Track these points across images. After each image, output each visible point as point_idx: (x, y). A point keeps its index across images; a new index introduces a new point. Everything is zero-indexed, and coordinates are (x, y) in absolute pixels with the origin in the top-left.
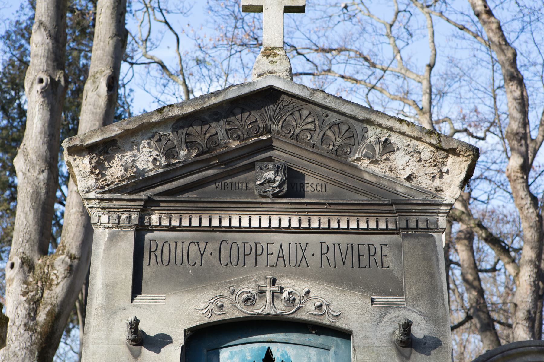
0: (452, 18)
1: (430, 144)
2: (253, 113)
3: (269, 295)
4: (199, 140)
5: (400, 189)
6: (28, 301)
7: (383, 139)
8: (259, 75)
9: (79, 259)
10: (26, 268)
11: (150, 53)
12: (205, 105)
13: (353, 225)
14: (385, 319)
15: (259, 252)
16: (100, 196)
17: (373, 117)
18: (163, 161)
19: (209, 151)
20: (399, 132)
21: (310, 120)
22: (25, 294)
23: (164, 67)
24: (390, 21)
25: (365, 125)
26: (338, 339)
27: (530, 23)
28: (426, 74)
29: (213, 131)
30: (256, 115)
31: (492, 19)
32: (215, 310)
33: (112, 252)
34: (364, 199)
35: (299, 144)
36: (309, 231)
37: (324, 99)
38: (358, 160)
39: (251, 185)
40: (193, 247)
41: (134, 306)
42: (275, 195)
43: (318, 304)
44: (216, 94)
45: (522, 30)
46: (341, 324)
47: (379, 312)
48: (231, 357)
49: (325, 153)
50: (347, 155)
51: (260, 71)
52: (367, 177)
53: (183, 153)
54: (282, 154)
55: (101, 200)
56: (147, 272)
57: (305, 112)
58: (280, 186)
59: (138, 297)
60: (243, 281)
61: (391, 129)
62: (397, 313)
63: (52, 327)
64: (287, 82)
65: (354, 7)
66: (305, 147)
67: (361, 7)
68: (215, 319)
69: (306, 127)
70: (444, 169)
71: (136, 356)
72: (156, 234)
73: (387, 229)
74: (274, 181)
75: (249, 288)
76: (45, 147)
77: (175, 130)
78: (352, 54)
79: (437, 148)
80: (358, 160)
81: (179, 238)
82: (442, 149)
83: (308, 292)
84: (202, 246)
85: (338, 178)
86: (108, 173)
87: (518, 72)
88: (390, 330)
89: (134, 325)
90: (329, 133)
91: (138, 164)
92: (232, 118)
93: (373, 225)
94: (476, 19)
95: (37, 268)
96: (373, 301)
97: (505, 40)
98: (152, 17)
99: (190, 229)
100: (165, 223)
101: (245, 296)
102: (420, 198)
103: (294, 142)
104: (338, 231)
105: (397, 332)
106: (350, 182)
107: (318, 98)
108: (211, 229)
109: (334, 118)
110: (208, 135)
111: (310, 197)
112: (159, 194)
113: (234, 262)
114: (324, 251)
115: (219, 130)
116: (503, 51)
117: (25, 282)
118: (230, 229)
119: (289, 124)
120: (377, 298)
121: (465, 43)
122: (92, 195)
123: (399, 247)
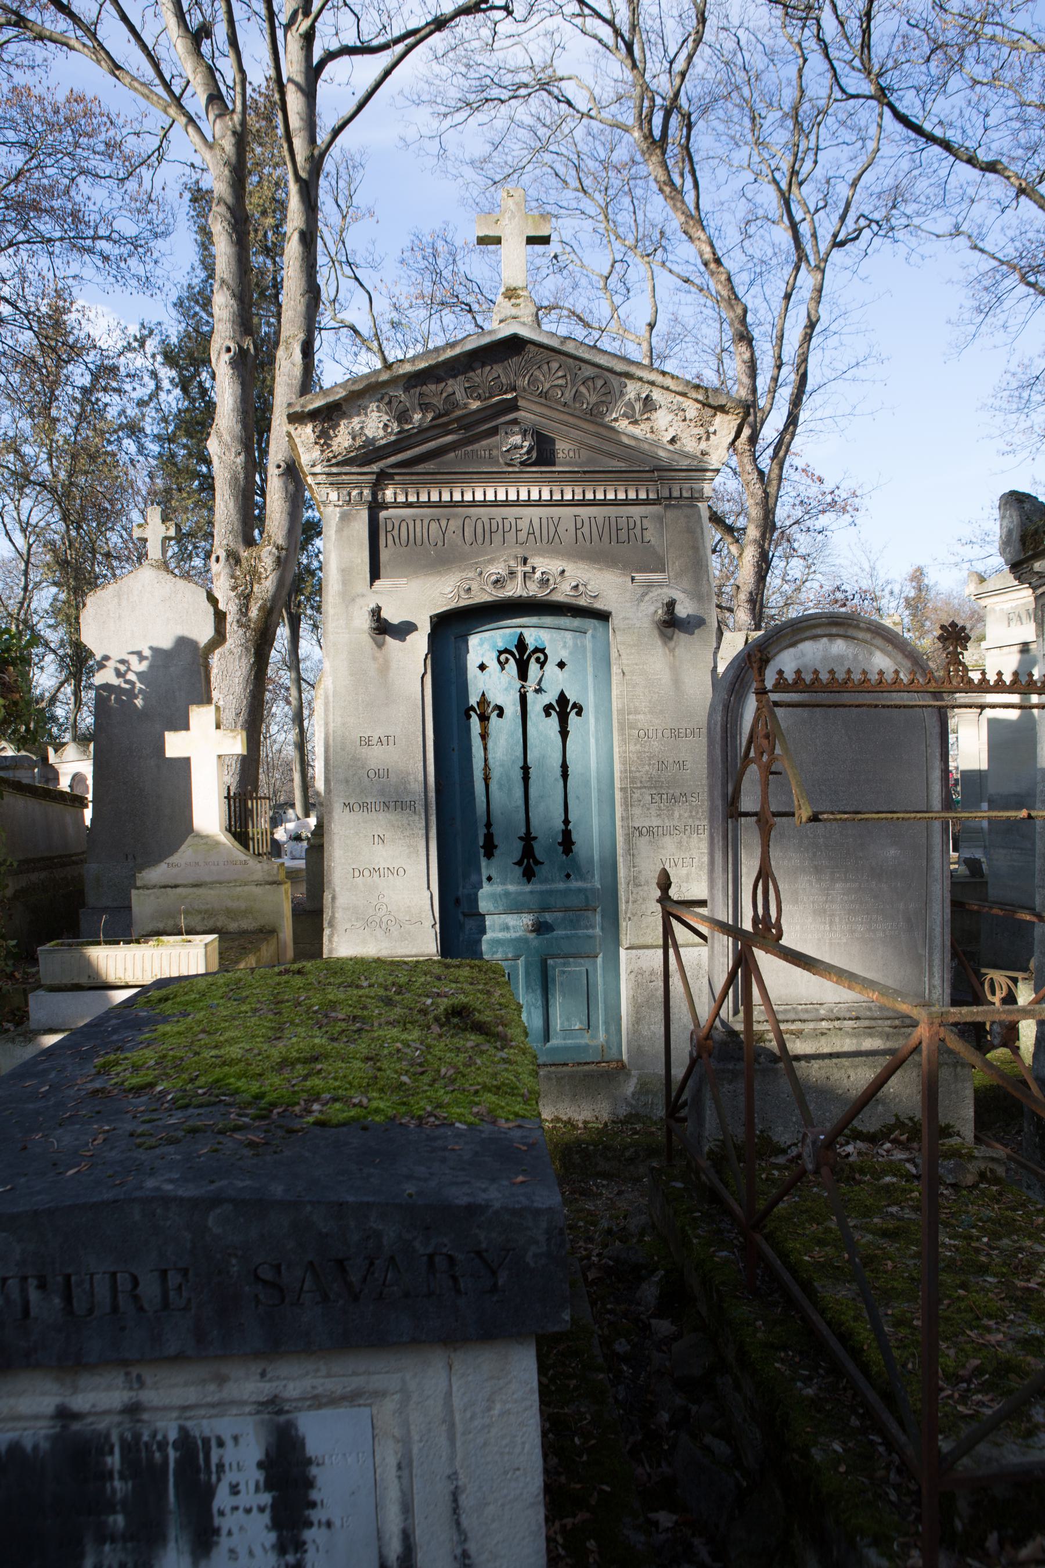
0: (676, 268)
1: (697, 400)
2: (495, 367)
3: (520, 575)
4: (434, 401)
5: (662, 453)
6: (238, 596)
7: (644, 396)
8: (501, 321)
9: (287, 550)
10: (232, 562)
11: (340, 316)
12: (440, 359)
13: (611, 496)
14: (647, 598)
15: (507, 529)
16: (327, 470)
17: (633, 370)
18: (395, 427)
19: (446, 414)
20: (662, 387)
21: (560, 374)
22: (234, 588)
23: (356, 331)
24: (606, 274)
25: (623, 379)
26: (595, 622)
27: (761, 273)
28: (647, 335)
29: (450, 390)
30: (498, 369)
31: (721, 269)
32: (462, 593)
33: (345, 533)
34: (622, 465)
35: (549, 403)
36: (562, 503)
37: (577, 349)
38: (616, 420)
39: (494, 452)
40: (434, 526)
41: (376, 592)
42: (523, 463)
43: (574, 584)
44: (452, 345)
45: (751, 284)
46: (599, 605)
47: (640, 591)
48: (481, 644)
49: (577, 413)
50: (603, 415)
51: (502, 316)
52: (625, 440)
53: (417, 417)
54: (529, 415)
55: (328, 474)
56: (384, 555)
57: (555, 365)
58: (528, 452)
59: (377, 583)
60: (491, 561)
61: (652, 383)
62: (660, 591)
63: (266, 622)
64: (534, 329)
65: (565, 257)
66: (555, 406)
67: (572, 256)
68: (463, 603)
69: (556, 383)
70: (711, 429)
71: (380, 645)
72: (391, 512)
73: (647, 499)
74: (522, 447)
75: (498, 569)
76: (240, 426)
77: (406, 390)
78: (565, 313)
79: (704, 405)
80: (616, 420)
81: (417, 516)
82: (710, 406)
83: (563, 571)
84: (444, 523)
85: (593, 441)
86: (334, 443)
87: (748, 332)
88: (652, 609)
89: (376, 612)
90: (583, 389)
91: (366, 431)
92: (471, 374)
93: (632, 495)
94: (702, 268)
95: (243, 561)
96: (633, 579)
97: (734, 293)
98: (339, 272)
99: (429, 504)
100: (401, 498)
101: (494, 578)
102: (684, 463)
103: (543, 401)
104: (594, 503)
105: (660, 612)
106: (607, 447)
107: (570, 348)
108: (452, 504)
109: (588, 371)
110: (444, 395)
111: (562, 465)
112: (392, 466)
113: (480, 540)
114: (579, 526)
115: (456, 388)
116: (732, 306)
117: (233, 577)
118: (474, 504)
119: (537, 380)
120: (636, 575)
121: (690, 298)
122: (318, 469)
123: (660, 519)
